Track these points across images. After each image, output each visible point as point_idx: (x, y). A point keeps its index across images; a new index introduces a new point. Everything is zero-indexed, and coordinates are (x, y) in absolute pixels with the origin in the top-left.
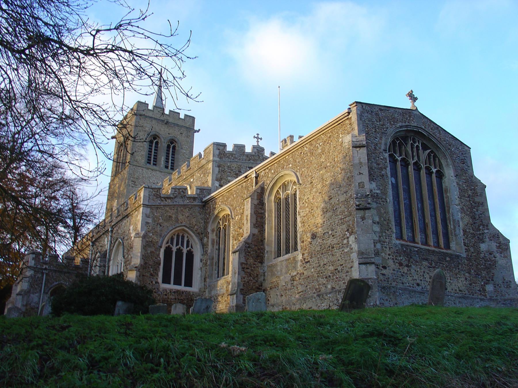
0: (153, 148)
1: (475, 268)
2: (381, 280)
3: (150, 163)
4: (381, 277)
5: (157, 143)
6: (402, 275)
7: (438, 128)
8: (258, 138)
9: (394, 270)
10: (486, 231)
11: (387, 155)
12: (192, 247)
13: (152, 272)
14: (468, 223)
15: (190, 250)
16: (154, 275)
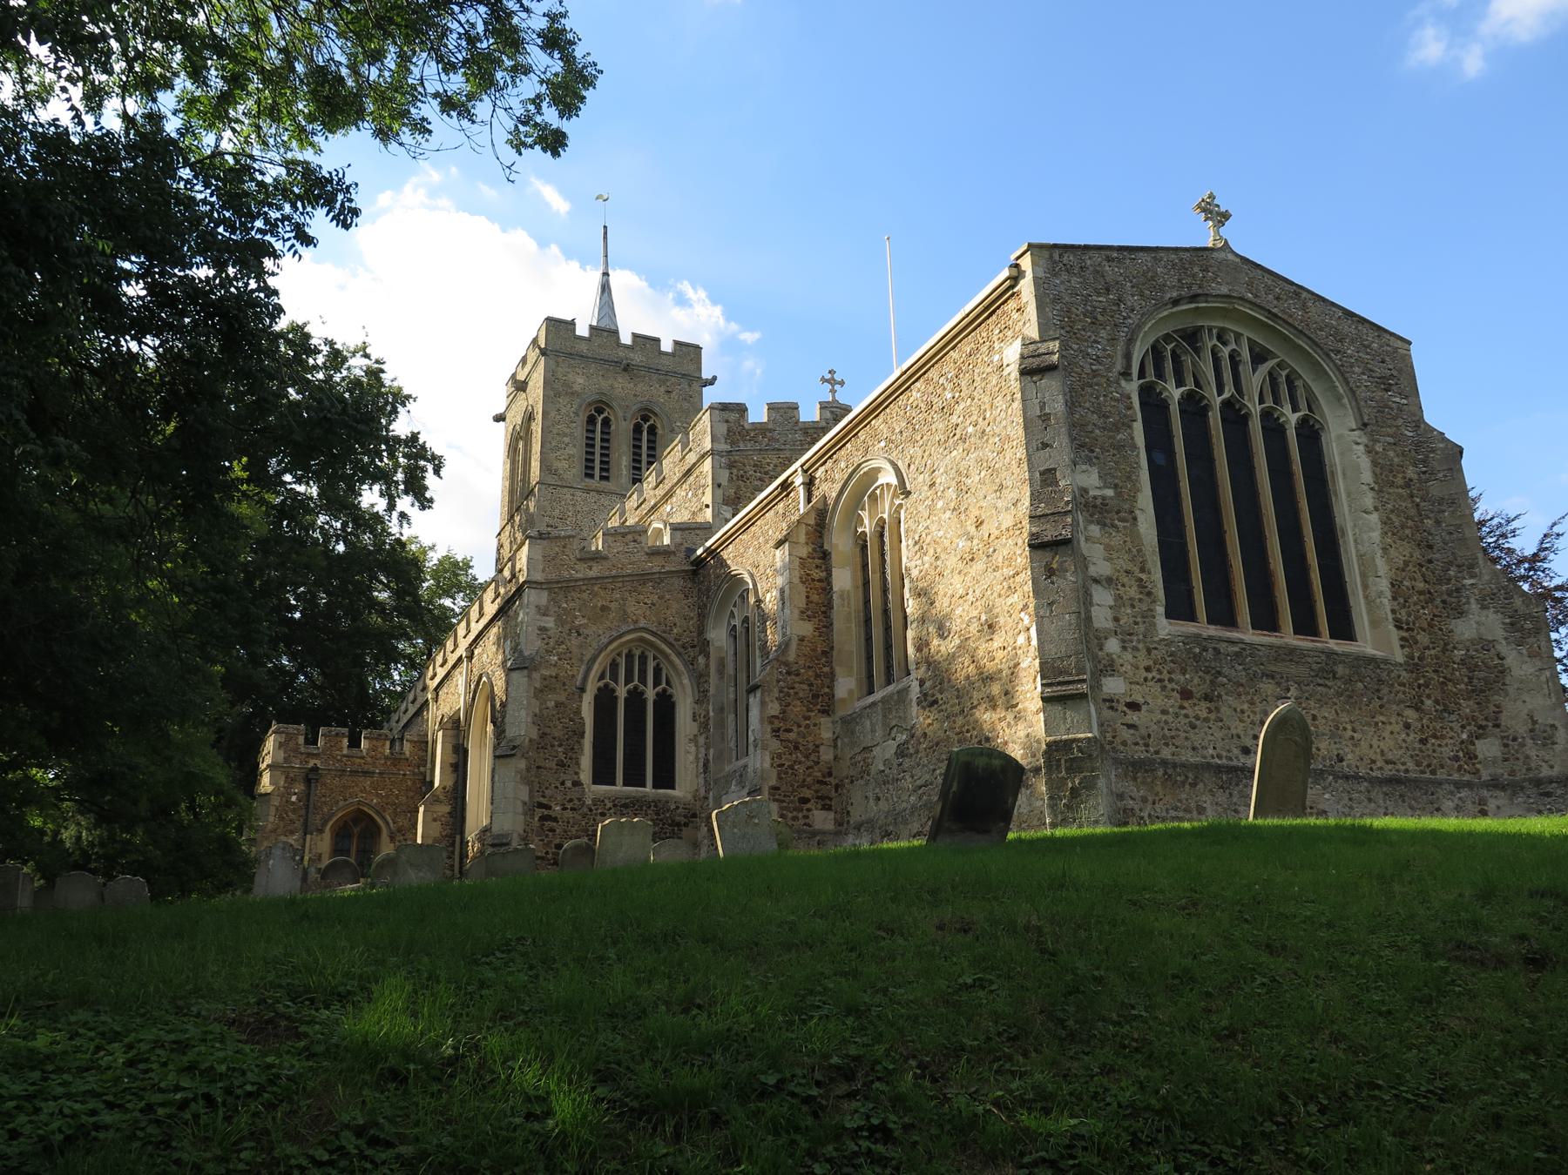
0: (598, 436)
1: (1437, 694)
2: (1124, 743)
3: (592, 476)
4: (1126, 734)
5: (606, 422)
6: (1194, 727)
7: (1297, 294)
8: (832, 382)
9: (1164, 712)
10: (1468, 582)
11: (1132, 387)
12: (668, 683)
13: (562, 756)
14: (1406, 563)
15: (664, 690)
16: (568, 763)
